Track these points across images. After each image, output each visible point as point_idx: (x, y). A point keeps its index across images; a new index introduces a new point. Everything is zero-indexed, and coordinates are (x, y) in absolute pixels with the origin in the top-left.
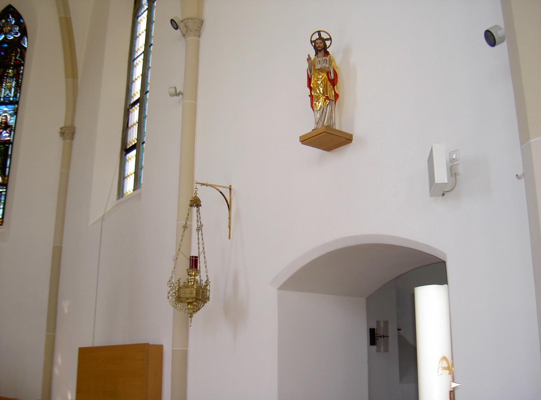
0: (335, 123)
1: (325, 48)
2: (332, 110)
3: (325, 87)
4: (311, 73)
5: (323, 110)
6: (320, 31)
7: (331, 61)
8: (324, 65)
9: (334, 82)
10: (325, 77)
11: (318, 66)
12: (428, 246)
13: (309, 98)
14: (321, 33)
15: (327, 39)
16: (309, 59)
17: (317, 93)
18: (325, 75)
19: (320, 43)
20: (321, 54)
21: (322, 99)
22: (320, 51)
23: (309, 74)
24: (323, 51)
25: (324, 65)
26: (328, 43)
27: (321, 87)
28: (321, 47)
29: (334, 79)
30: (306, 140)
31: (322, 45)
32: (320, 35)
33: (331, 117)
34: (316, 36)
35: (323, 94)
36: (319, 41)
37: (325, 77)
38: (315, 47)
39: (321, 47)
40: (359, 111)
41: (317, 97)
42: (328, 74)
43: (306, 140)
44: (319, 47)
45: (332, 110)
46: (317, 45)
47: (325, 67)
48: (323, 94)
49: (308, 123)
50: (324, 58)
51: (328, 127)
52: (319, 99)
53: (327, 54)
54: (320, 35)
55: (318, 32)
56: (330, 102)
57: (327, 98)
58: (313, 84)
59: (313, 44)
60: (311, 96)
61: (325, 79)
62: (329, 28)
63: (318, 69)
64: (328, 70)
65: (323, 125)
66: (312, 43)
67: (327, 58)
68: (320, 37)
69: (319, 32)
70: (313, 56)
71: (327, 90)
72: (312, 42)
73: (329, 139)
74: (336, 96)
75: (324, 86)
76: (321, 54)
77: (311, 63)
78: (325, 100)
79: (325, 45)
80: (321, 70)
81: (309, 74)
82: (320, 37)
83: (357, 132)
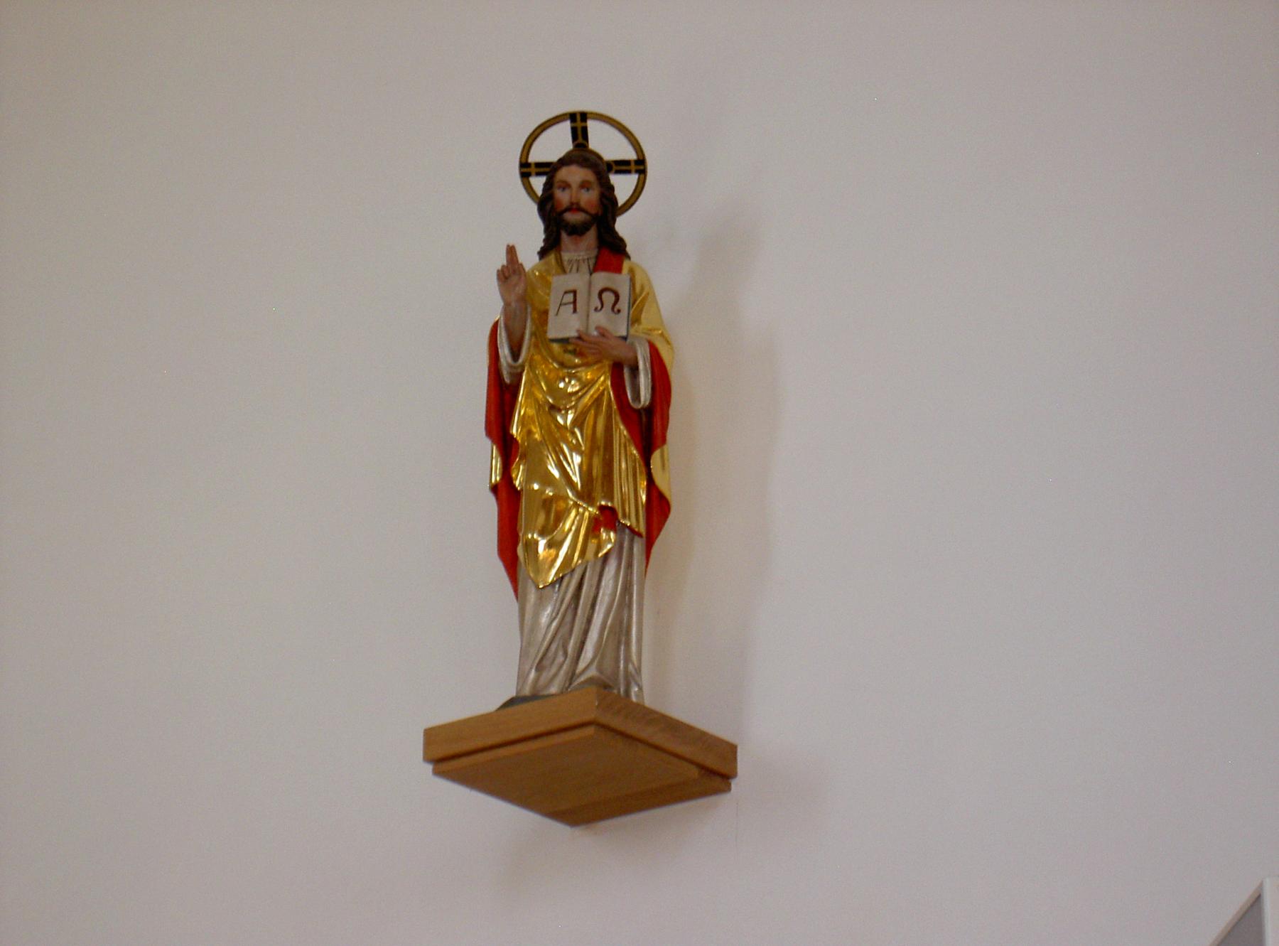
0: (638, 670)
1: (609, 208)
2: (627, 588)
3: (601, 450)
4: (515, 354)
5: (576, 590)
6: (584, 116)
7: (639, 300)
8: (599, 319)
9: (648, 428)
10: (587, 378)
11: (564, 324)
12: (735, 759)
13: (492, 500)
14: (592, 125)
15: (622, 166)
16: (510, 272)
17: (547, 479)
18: (604, 381)
19: (585, 185)
20: (579, 251)
21: (574, 521)
22: (577, 231)
23: (504, 352)
24: (591, 235)
25: (599, 319)
26: (623, 185)
27: (576, 448)
28: (582, 204)
29: (650, 410)
30: (460, 755)
31: (589, 198)
32: (580, 135)
33: (619, 632)
34: (556, 145)
35: (586, 495)
36: (574, 175)
37: (587, 378)
38: (546, 206)
39: (582, 204)
40: (775, 609)
41: (547, 504)
42: (620, 370)
43: (460, 755)
44: (574, 207)
45: (627, 588)
46: (563, 197)
47: (603, 333)
48: (586, 495)
49: (478, 657)
50: (602, 279)
51: (603, 686)
52: (560, 517)
53: (612, 251)
54: (580, 135)
55: (572, 117)
56: (619, 544)
57: (608, 518)
58: (523, 422)
59: (538, 183)
60: (506, 494)
61: (597, 401)
62: (636, 102)
63: (564, 341)
64: (621, 352)
65: (572, 676)
66: (525, 176)
67: (620, 282)
68: (581, 153)
69: (579, 122)
70: (529, 259)
71: (608, 465)
72: (527, 169)
73: (597, 758)
74: (658, 507)
75: (593, 448)
76: (579, 251)
77: (524, 299)
78: (595, 527)
79: (607, 191)
80: (580, 348)
81: (504, 352)
82: (581, 153)
83: (764, 730)
